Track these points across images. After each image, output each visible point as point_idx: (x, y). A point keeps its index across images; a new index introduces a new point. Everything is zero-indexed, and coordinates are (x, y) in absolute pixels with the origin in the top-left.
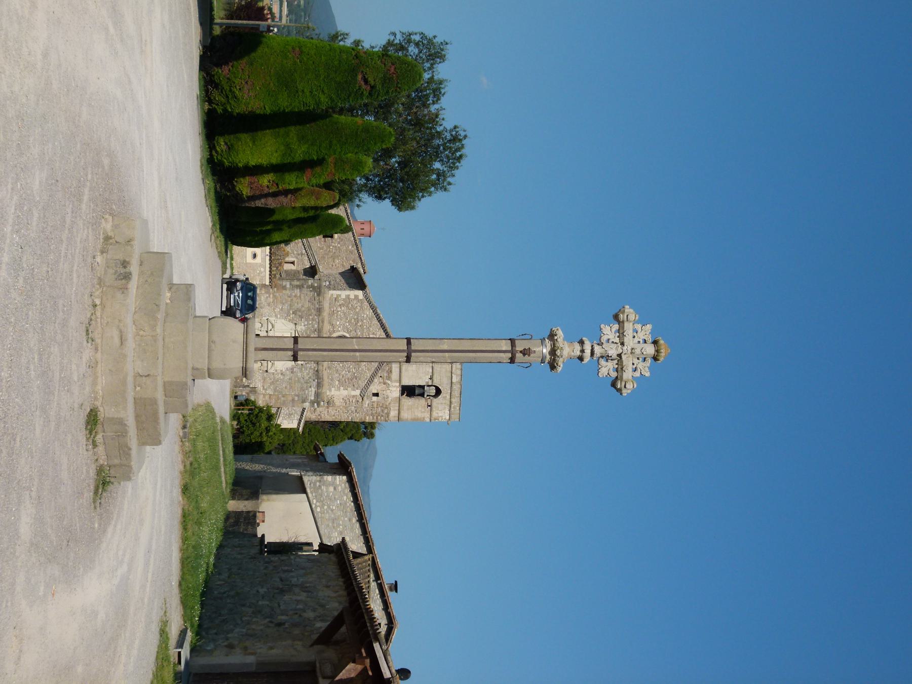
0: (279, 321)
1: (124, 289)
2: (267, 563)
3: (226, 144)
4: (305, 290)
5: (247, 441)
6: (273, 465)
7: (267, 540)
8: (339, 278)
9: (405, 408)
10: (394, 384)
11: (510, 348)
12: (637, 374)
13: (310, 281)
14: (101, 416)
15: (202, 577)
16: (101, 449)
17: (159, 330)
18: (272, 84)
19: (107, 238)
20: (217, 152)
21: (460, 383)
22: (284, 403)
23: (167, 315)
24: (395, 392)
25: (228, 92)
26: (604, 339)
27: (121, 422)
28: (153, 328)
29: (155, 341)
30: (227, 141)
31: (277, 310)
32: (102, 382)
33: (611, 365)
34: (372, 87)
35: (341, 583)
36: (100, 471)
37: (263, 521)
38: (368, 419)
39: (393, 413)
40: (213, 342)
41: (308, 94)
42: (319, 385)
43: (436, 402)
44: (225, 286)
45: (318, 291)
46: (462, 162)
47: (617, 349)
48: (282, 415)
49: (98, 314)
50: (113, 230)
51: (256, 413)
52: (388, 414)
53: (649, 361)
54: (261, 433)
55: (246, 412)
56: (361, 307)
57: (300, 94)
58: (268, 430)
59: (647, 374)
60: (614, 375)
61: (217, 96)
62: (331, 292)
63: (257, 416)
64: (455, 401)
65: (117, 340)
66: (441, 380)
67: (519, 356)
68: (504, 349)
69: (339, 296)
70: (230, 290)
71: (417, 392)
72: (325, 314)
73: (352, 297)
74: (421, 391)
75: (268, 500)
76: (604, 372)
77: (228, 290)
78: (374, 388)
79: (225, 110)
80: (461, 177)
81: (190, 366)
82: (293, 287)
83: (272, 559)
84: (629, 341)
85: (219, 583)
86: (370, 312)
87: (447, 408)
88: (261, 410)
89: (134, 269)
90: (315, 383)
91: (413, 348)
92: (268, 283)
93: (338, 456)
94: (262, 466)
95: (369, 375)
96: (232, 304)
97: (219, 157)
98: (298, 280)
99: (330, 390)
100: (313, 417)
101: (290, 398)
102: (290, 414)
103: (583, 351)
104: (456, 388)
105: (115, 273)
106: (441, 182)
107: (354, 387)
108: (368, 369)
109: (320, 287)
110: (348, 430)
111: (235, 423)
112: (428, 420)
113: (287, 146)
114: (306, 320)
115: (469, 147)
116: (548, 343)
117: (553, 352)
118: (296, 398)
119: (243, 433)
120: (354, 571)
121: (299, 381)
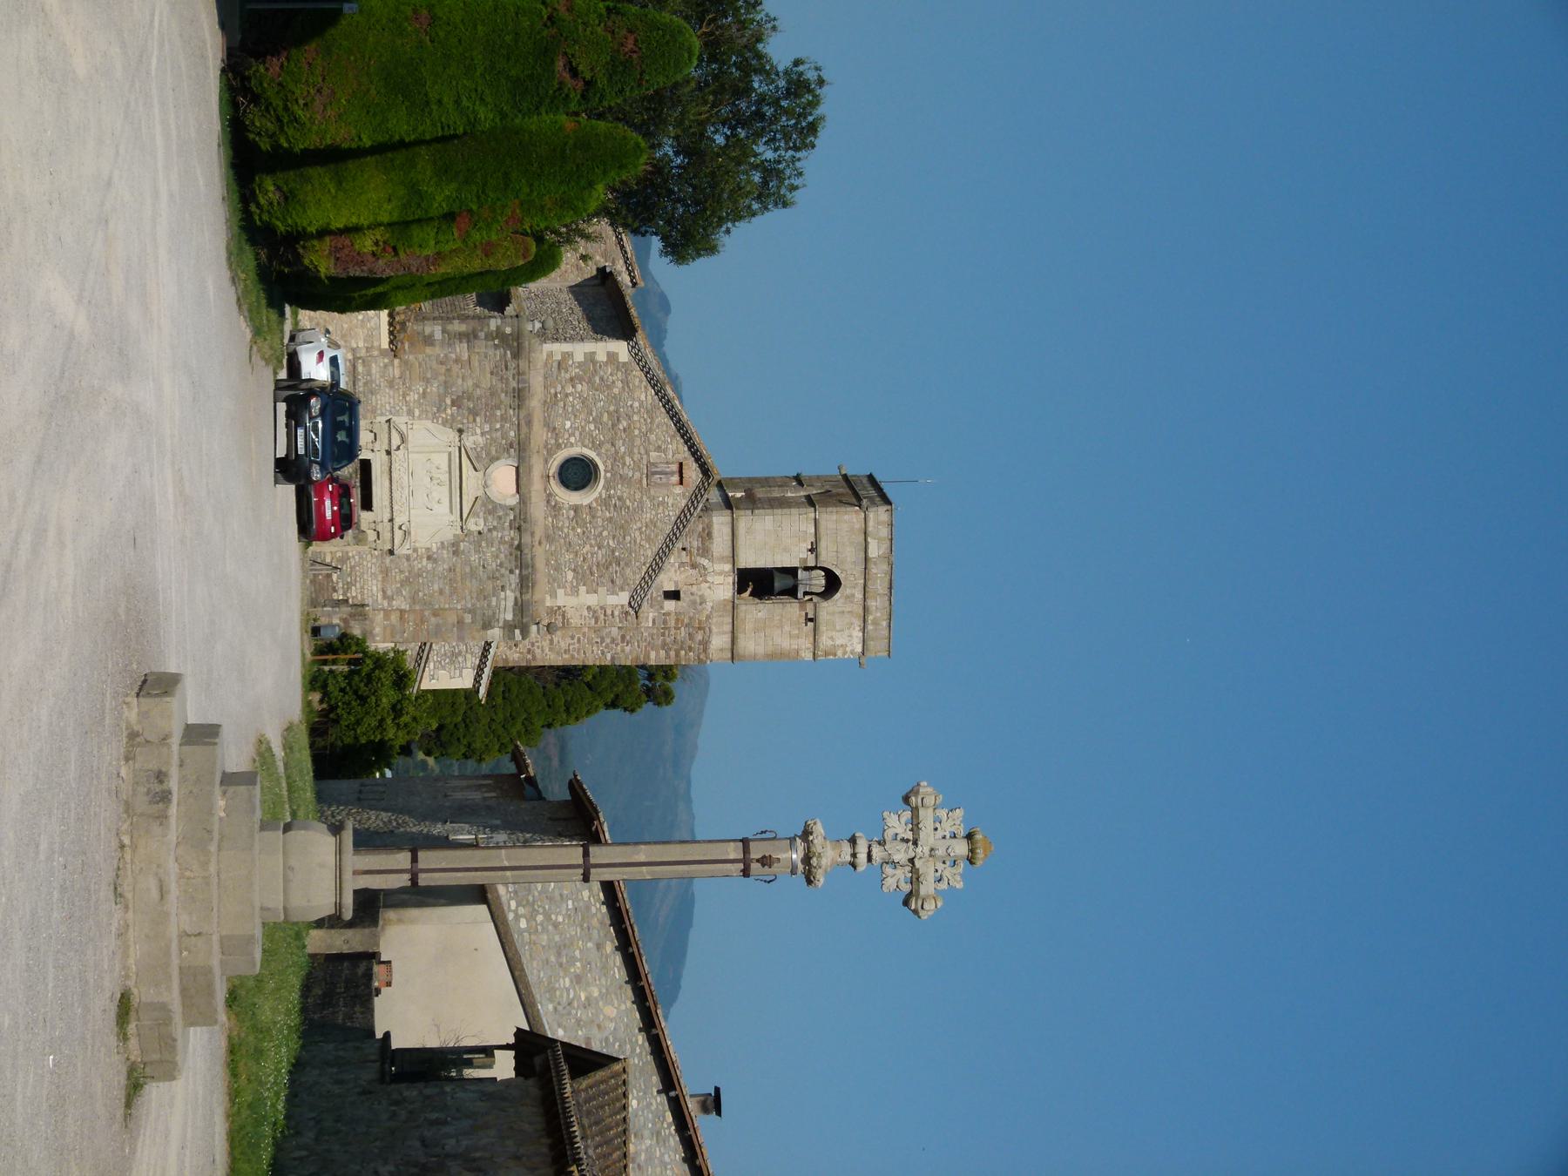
0: (418, 425)
1: (162, 818)
2: (397, 1103)
3: (279, 188)
4: (481, 346)
5: (348, 740)
6: (410, 813)
7: (396, 1044)
8: (567, 297)
9: (749, 626)
10: (719, 567)
11: (741, 856)
12: (943, 886)
13: (494, 324)
14: (135, 1001)
15: (266, 1156)
16: (133, 1043)
17: (212, 869)
18: (373, 92)
19: (133, 735)
20: (258, 205)
21: (889, 558)
22: (438, 632)
23: (221, 840)
24: (721, 587)
25: (280, 111)
26: (889, 834)
27: (164, 1007)
28: (205, 865)
29: (208, 884)
30: (280, 183)
31: (413, 397)
32: (135, 952)
33: (902, 874)
34: (589, 84)
35: (545, 1150)
36: (132, 1069)
37: (389, 984)
38: (655, 658)
39: (719, 641)
40: (292, 869)
41: (451, 106)
42: (525, 583)
43: (827, 609)
44: (282, 407)
45: (515, 346)
46: (821, 133)
47: (906, 851)
48: (434, 657)
49: (128, 857)
50: (139, 722)
51: (365, 670)
52: (705, 644)
53: (962, 865)
54: (382, 721)
55: (342, 668)
56: (626, 382)
57: (434, 107)
58: (397, 710)
59: (960, 885)
60: (906, 888)
61: (258, 121)
62: (548, 347)
63: (369, 678)
64: (877, 605)
65: (155, 894)
66: (840, 554)
67: (755, 867)
68: (732, 857)
69: (567, 356)
70: (296, 414)
71: (778, 585)
72: (535, 403)
73: (602, 357)
74: (789, 582)
75: (400, 921)
76: (890, 883)
77: (289, 415)
78: (667, 581)
79: (277, 147)
80: (817, 168)
81: (257, 905)
82: (452, 338)
83: (406, 1094)
84: (927, 837)
85: (297, 1154)
86: (646, 395)
87: (858, 623)
88: (379, 661)
89: (173, 784)
90: (514, 579)
91: (592, 861)
92: (385, 344)
93: (571, 782)
94: (385, 816)
95: (650, 553)
96: (301, 451)
97: (265, 217)
98: (464, 318)
99: (554, 595)
100: (515, 657)
101: (452, 619)
102: (454, 655)
103: (854, 855)
104: (879, 571)
105: (148, 793)
106: (773, 189)
107: (614, 586)
108: (648, 539)
109: (518, 336)
110: (605, 684)
111: (316, 697)
112: (808, 656)
113: (414, 190)
114: (489, 419)
115: (830, 106)
116: (800, 844)
117: (807, 859)
118: (468, 618)
119: (336, 721)
120: (570, 1125)
121: (473, 574)
